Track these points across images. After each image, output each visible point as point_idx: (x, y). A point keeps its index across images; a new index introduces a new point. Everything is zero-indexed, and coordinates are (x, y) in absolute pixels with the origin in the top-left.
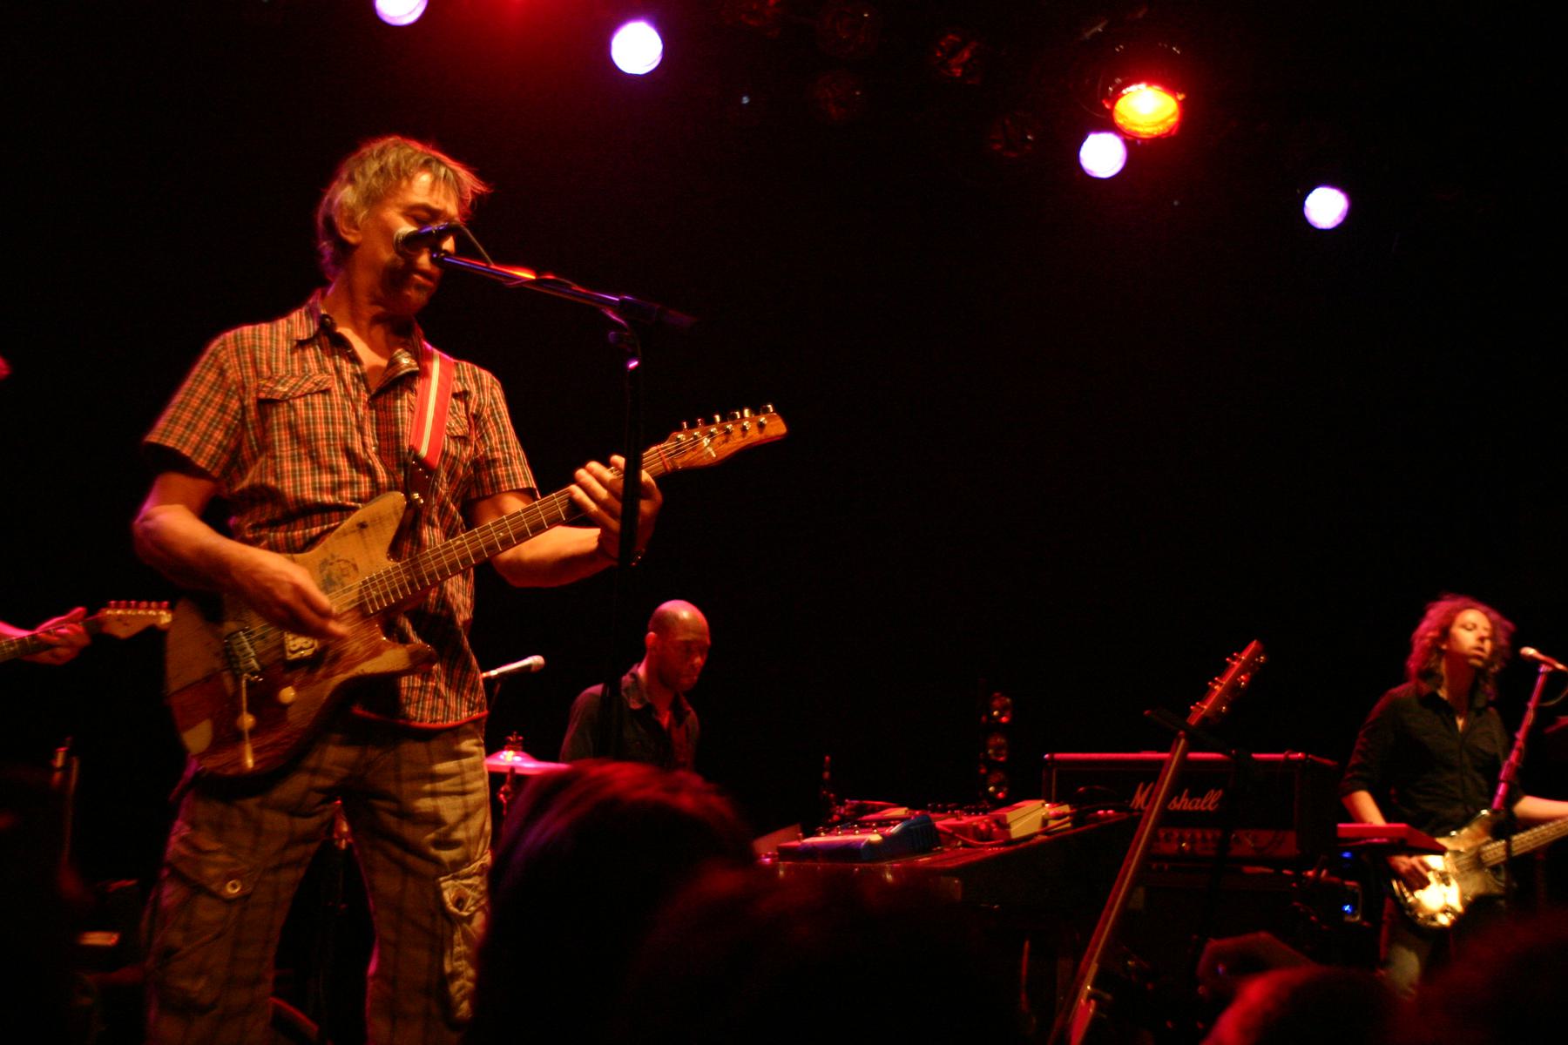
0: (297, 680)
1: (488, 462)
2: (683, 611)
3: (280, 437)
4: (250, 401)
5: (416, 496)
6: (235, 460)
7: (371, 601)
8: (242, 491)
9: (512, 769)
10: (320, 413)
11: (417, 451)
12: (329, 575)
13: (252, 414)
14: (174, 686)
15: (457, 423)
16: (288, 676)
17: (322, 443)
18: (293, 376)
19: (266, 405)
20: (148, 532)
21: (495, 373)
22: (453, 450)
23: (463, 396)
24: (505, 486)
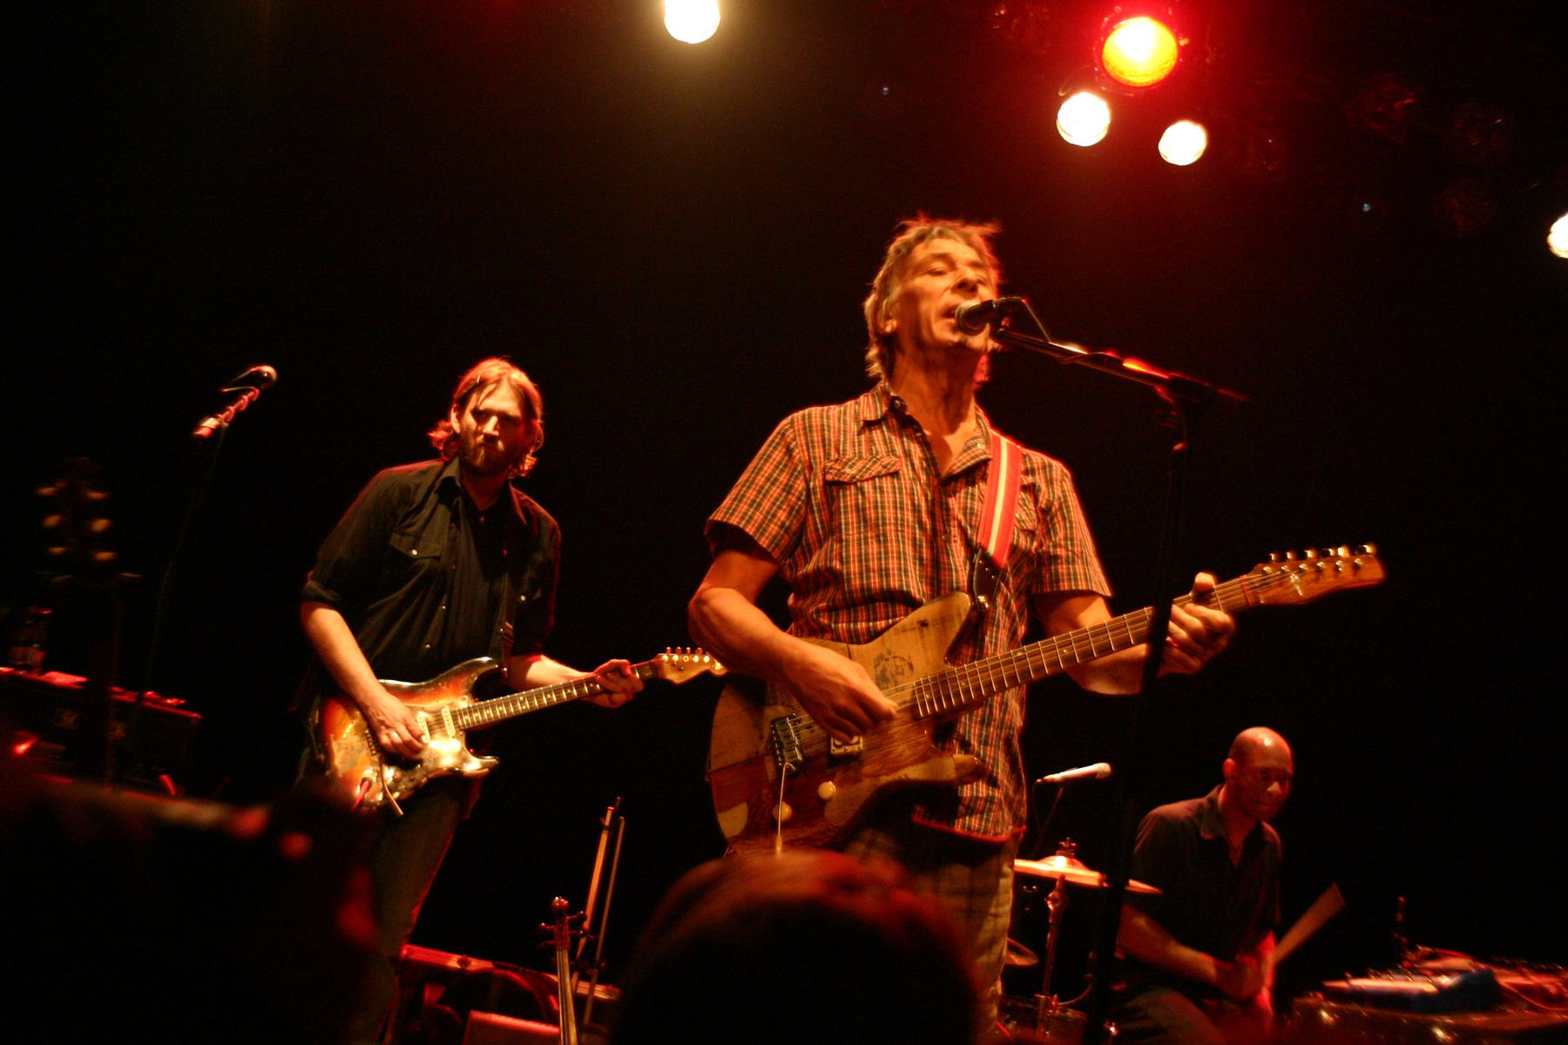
0: (838, 776)
1: (1050, 557)
2: (1265, 737)
3: (848, 520)
4: (816, 483)
6: (797, 542)
8: (806, 576)
11: (984, 549)
12: (884, 671)
13: (817, 498)
14: (715, 764)
15: (1026, 515)
16: (830, 771)
17: (890, 528)
19: (834, 487)
21: (1068, 463)
23: (1031, 489)
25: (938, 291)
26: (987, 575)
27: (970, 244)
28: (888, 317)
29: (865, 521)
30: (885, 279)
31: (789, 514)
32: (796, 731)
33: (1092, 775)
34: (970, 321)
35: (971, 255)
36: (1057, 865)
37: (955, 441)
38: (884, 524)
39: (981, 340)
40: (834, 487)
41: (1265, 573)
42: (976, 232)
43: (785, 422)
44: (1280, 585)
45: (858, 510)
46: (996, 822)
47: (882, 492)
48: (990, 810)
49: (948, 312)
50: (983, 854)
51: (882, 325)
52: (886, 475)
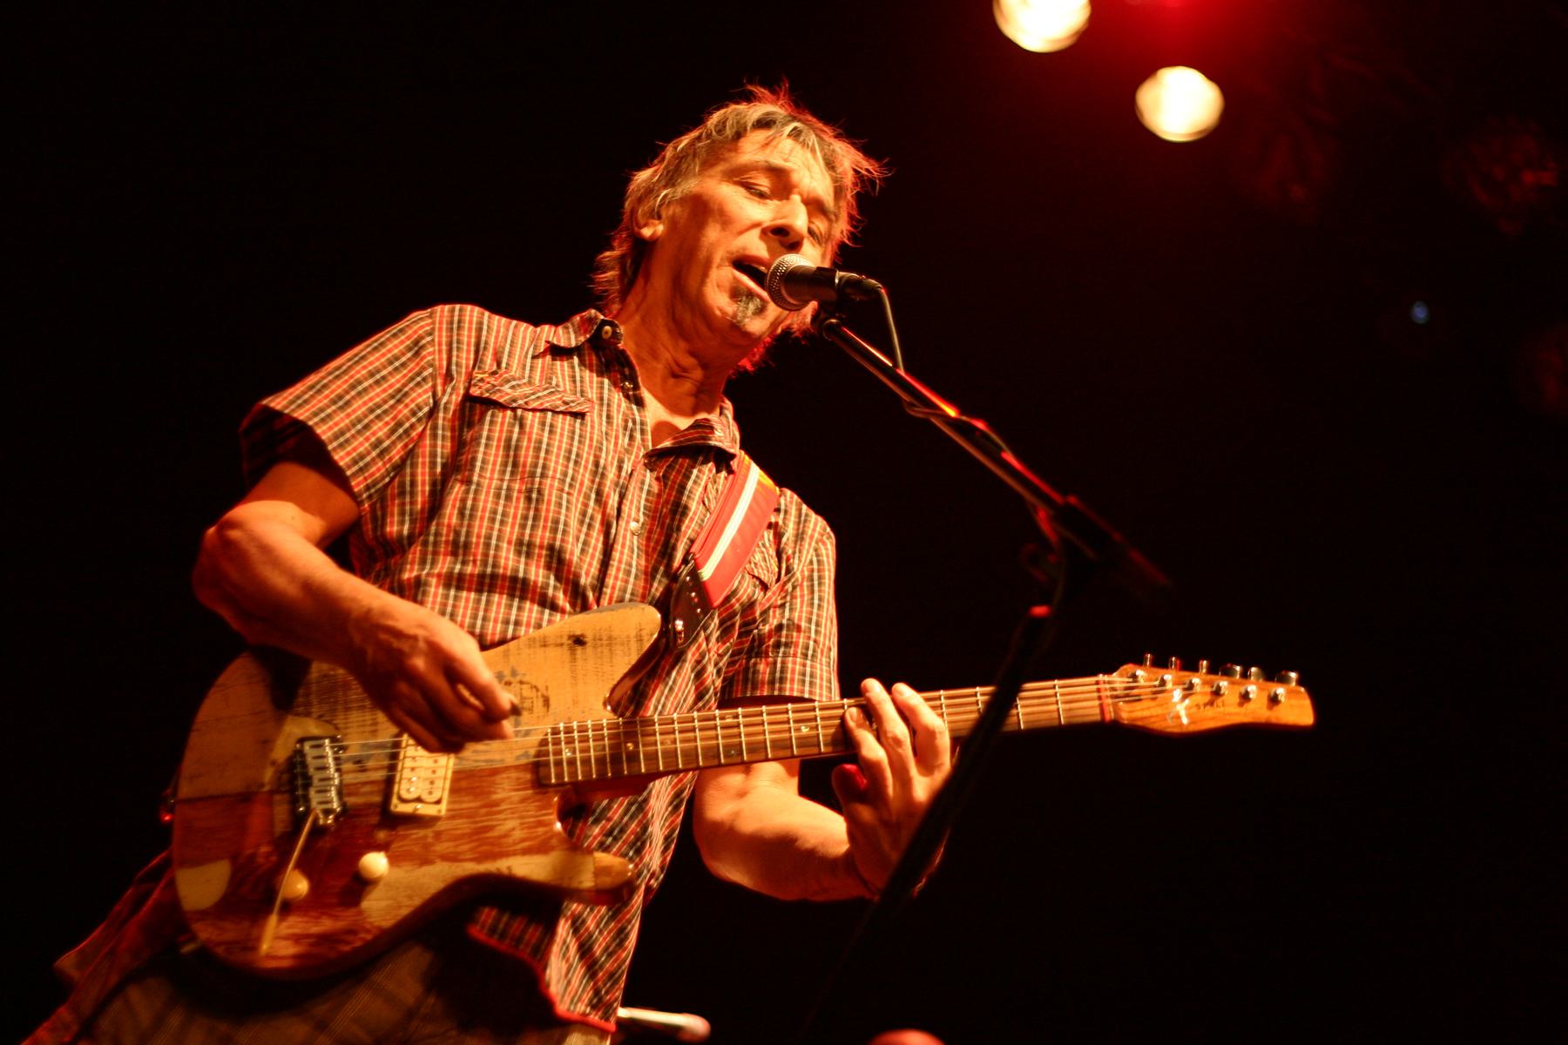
4: (452, 398)
5: (679, 624)
7: (559, 763)
10: (561, 441)
16: (382, 835)
20: (228, 545)
27: (830, 165)
29: (515, 465)
30: (681, 158)
33: (676, 1030)
38: (543, 476)
40: (475, 408)
42: (849, 158)
45: (508, 447)
49: (743, 263)
52: (564, 413)
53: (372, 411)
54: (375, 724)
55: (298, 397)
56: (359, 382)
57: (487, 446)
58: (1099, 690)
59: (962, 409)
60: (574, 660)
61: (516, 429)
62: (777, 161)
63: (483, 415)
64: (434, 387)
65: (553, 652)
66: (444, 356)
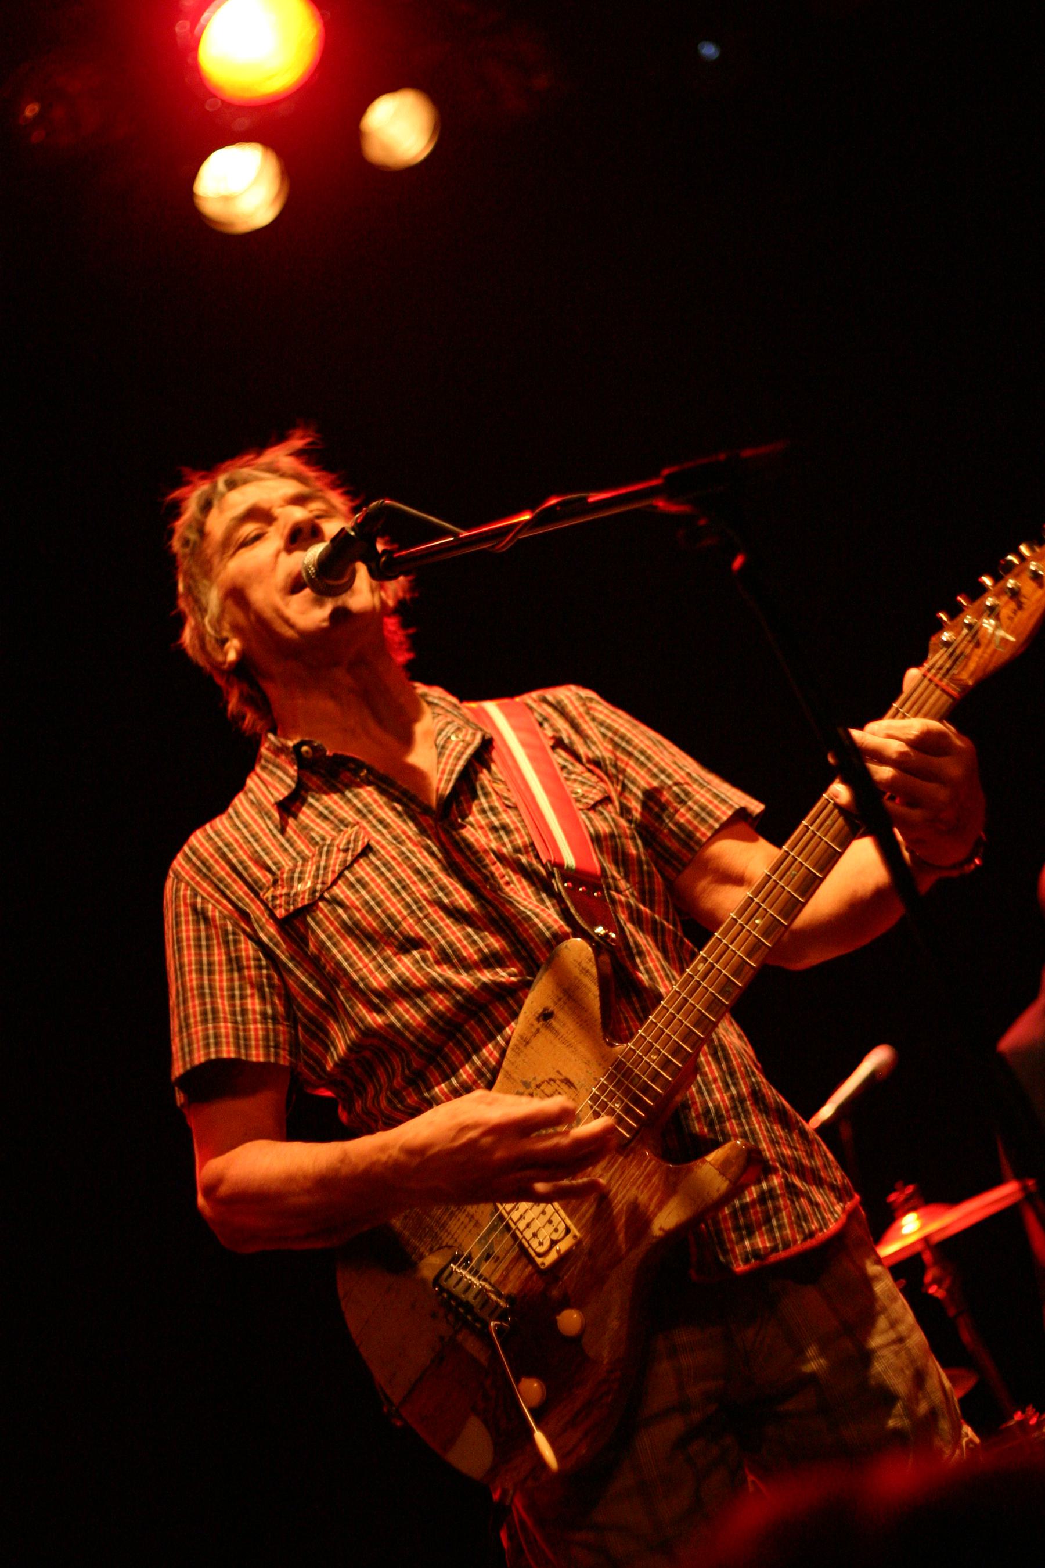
4: (268, 933)
9: (926, 1240)
10: (378, 886)
11: (560, 865)
18: (305, 860)
19: (294, 924)
22: (603, 828)
24: (704, 832)
25: (267, 567)
26: (582, 895)
27: (274, 470)
28: (223, 642)
31: (263, 998)
32: (475, 1273)
34: (328, 579)
35: (291, 488)
36: (911, 1227)
37: (421, 757)
38: (397, 925)
39: (363, 593)
40: (294, 924)
41: (947, 644)
42: (281, 456)
43: (169, 883)
44: (978, 645)
46: (801, 1218)
47: (365, 886)
48: (777, 1210)
49: (295, 585)
50: (832, 1267)
51: (220, 658)
52: (355, 860)
53: (232, 997)
54: (472, 1217)
55: (182, 1049)
56: (201, 987)
57: (335, 945)
58: (931, 681)
59: (531, 508)
60: (556, 1033)
61: (340, 911)
62: (241, 509)
63: (307, 926)
64: (244, 931)
65: (538, 1042)
66: (225, 902)
